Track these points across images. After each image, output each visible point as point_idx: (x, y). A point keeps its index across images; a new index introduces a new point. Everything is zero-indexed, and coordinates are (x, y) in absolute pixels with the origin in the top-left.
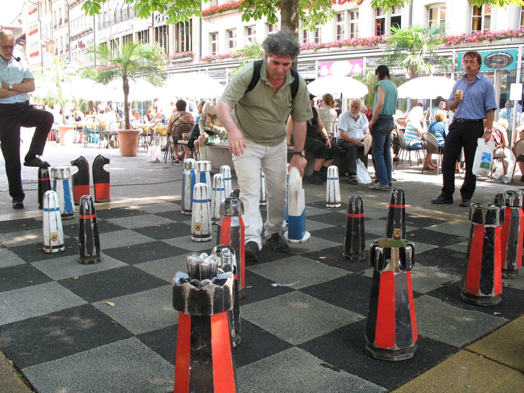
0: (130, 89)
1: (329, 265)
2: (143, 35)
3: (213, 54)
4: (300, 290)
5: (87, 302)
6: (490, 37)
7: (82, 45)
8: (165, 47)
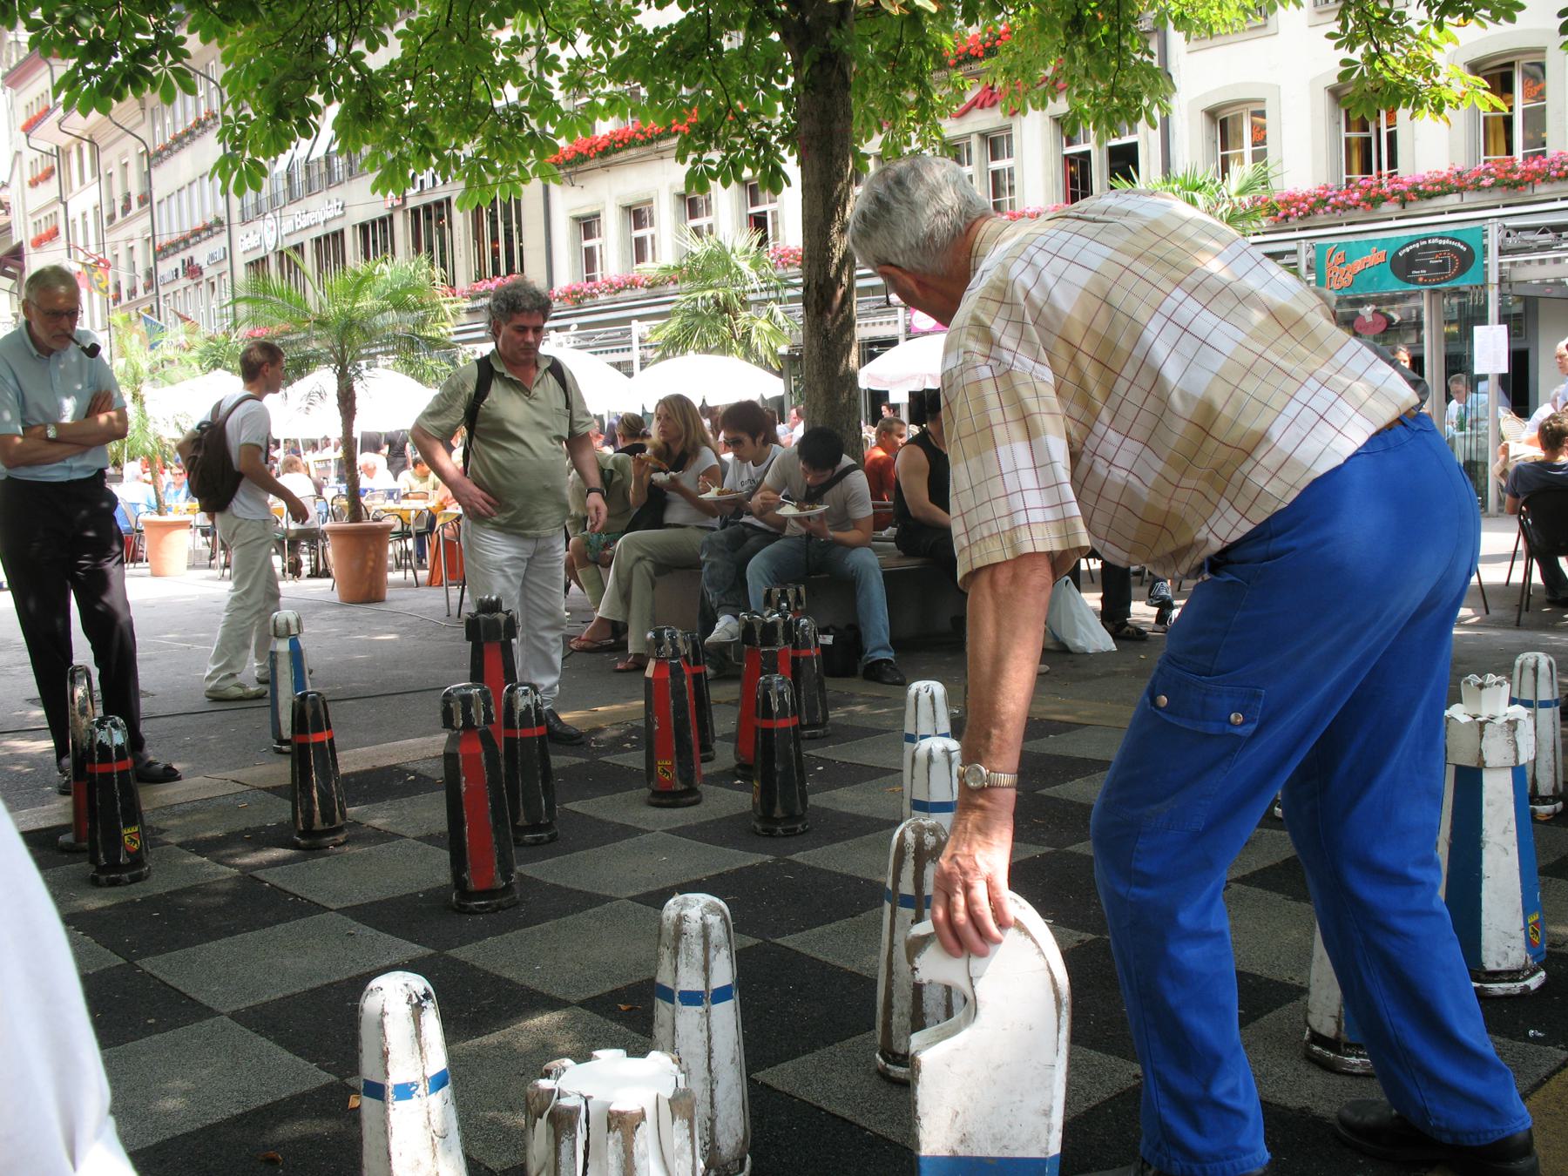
0: (358, 403)
2: (375, 234)
5: (333, 1078)
6: (1400, 192)
7: (192, 270)
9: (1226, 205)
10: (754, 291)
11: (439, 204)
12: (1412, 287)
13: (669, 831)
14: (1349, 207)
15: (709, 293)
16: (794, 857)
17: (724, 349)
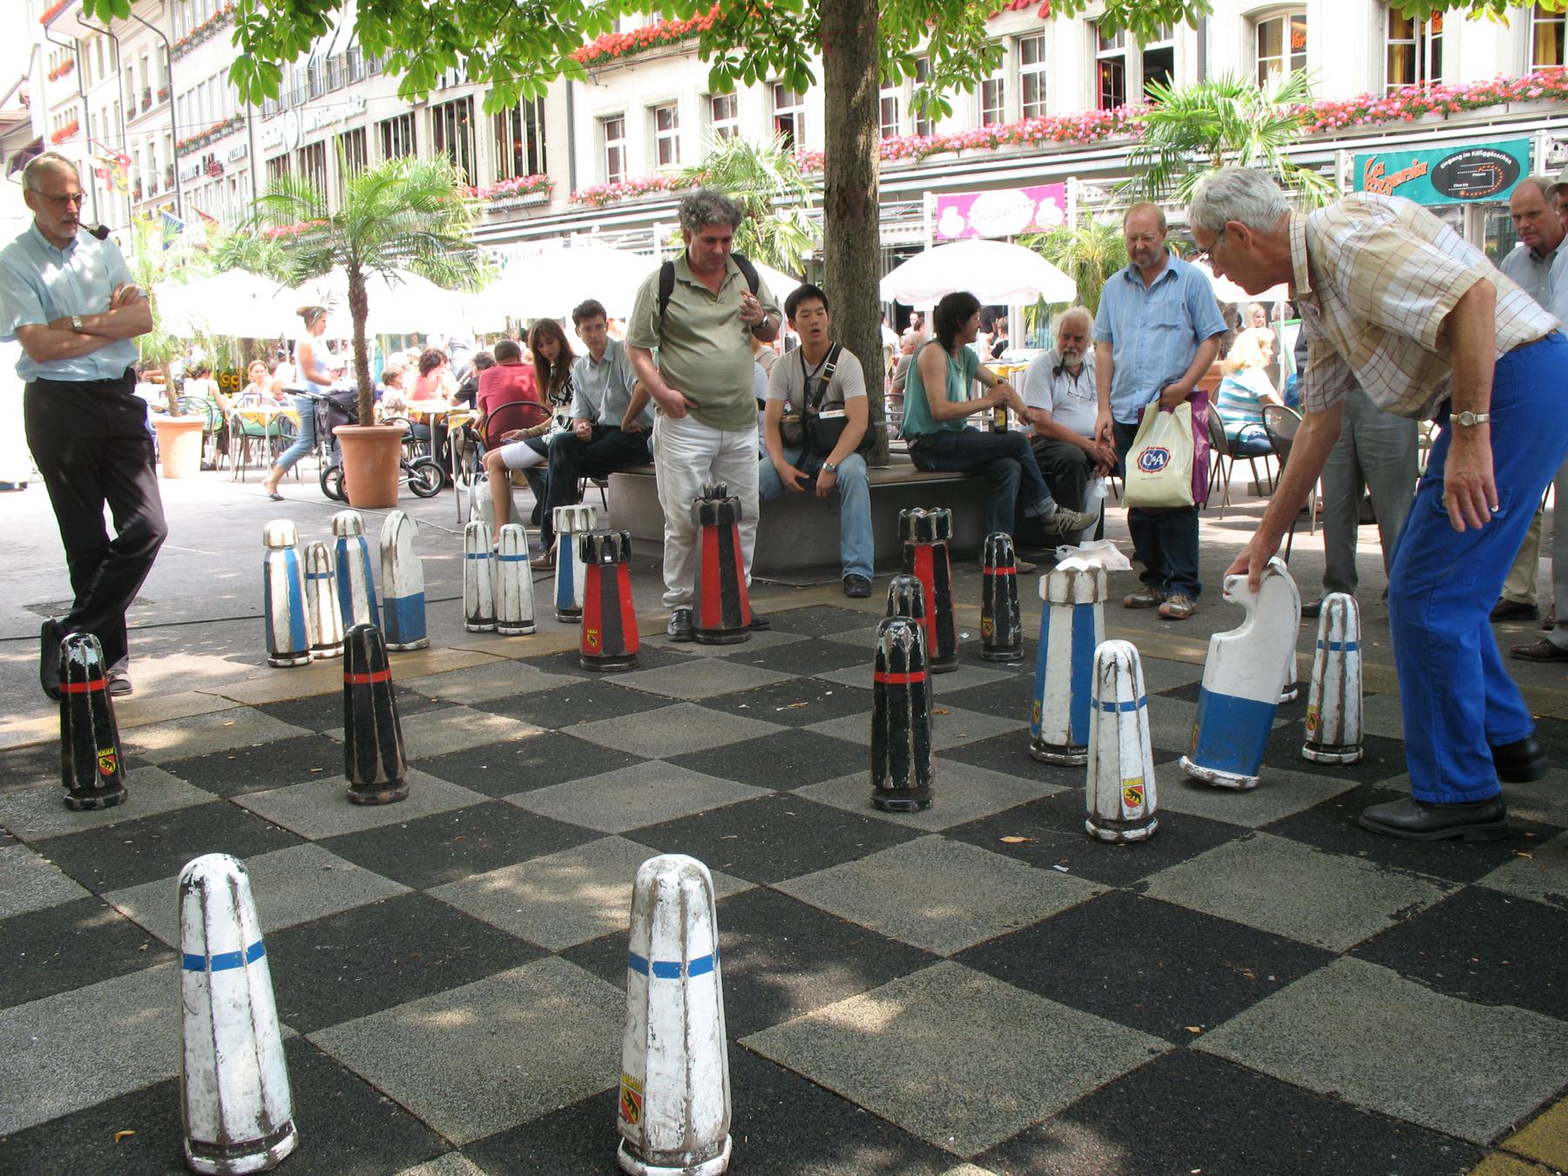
0: (370, 304)
1: (1033, 866)
2: (396, 132)
3: (612, 181)
4: (954, 957)
6: (1444, 102)
7: (213, 167)
8: (466, 166)
9: (1263, 113)
10: (779, 195)
11: (461, 102)
12: (1453, 201)
13: (666, 760)
14: (1390, 117)
16: (796, 791)
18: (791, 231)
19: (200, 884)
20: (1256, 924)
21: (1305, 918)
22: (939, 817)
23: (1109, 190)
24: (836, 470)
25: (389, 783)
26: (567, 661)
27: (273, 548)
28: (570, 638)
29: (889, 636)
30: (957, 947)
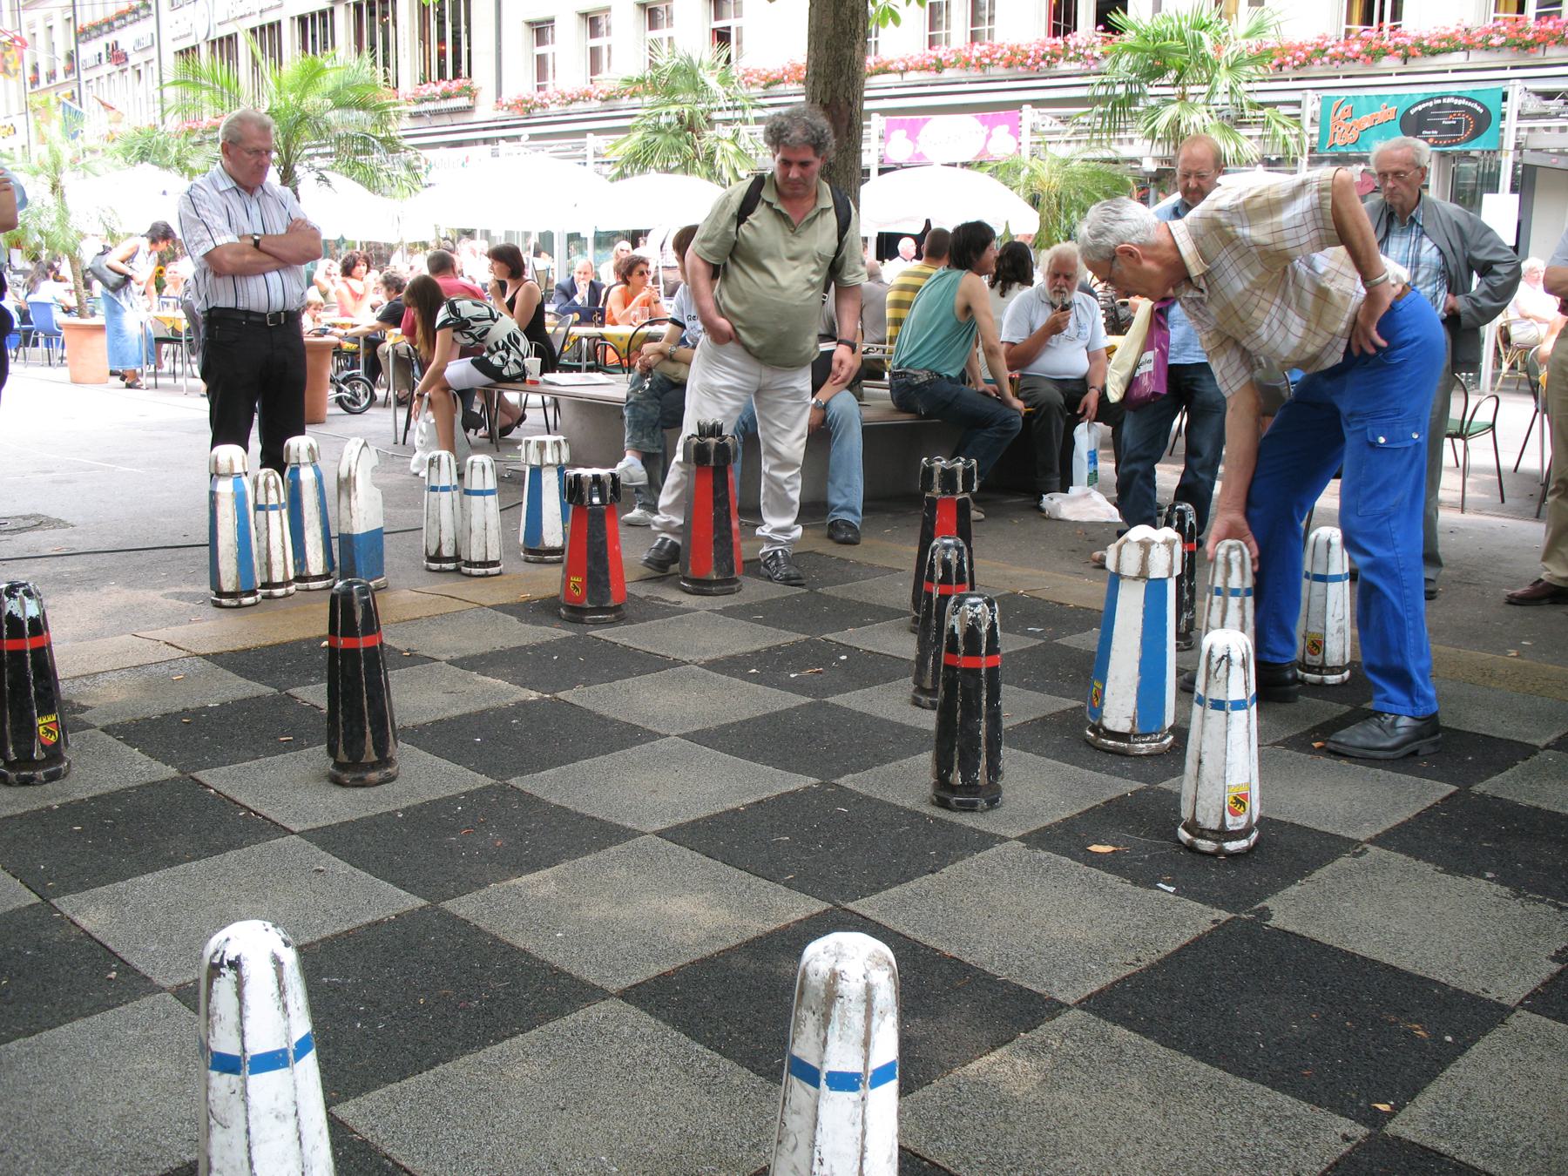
1: (1135, 883)
13: (684, 736)
15: (674, 109)
16: (842, 781)
17: (686, 167)
18: (732, 148)
19: (235, 965)
20: (1407, 966)
21: (1459, 958)
22: (1013, 818)
23: (1064, 120)
24: (825, 407)
25: (379, 762)
26: (545, 609)
27: (219, 475)
28: (550, 580)
29: (964, 615)
30: (1083, 993)
